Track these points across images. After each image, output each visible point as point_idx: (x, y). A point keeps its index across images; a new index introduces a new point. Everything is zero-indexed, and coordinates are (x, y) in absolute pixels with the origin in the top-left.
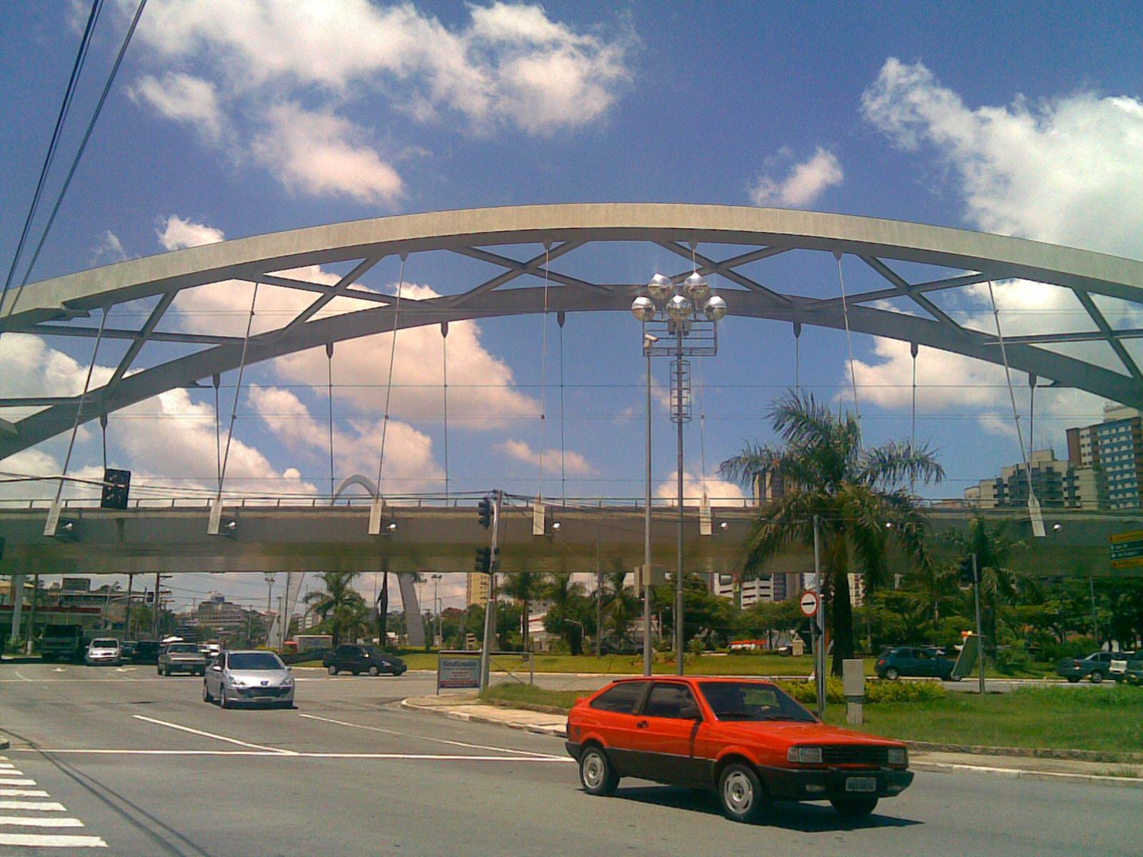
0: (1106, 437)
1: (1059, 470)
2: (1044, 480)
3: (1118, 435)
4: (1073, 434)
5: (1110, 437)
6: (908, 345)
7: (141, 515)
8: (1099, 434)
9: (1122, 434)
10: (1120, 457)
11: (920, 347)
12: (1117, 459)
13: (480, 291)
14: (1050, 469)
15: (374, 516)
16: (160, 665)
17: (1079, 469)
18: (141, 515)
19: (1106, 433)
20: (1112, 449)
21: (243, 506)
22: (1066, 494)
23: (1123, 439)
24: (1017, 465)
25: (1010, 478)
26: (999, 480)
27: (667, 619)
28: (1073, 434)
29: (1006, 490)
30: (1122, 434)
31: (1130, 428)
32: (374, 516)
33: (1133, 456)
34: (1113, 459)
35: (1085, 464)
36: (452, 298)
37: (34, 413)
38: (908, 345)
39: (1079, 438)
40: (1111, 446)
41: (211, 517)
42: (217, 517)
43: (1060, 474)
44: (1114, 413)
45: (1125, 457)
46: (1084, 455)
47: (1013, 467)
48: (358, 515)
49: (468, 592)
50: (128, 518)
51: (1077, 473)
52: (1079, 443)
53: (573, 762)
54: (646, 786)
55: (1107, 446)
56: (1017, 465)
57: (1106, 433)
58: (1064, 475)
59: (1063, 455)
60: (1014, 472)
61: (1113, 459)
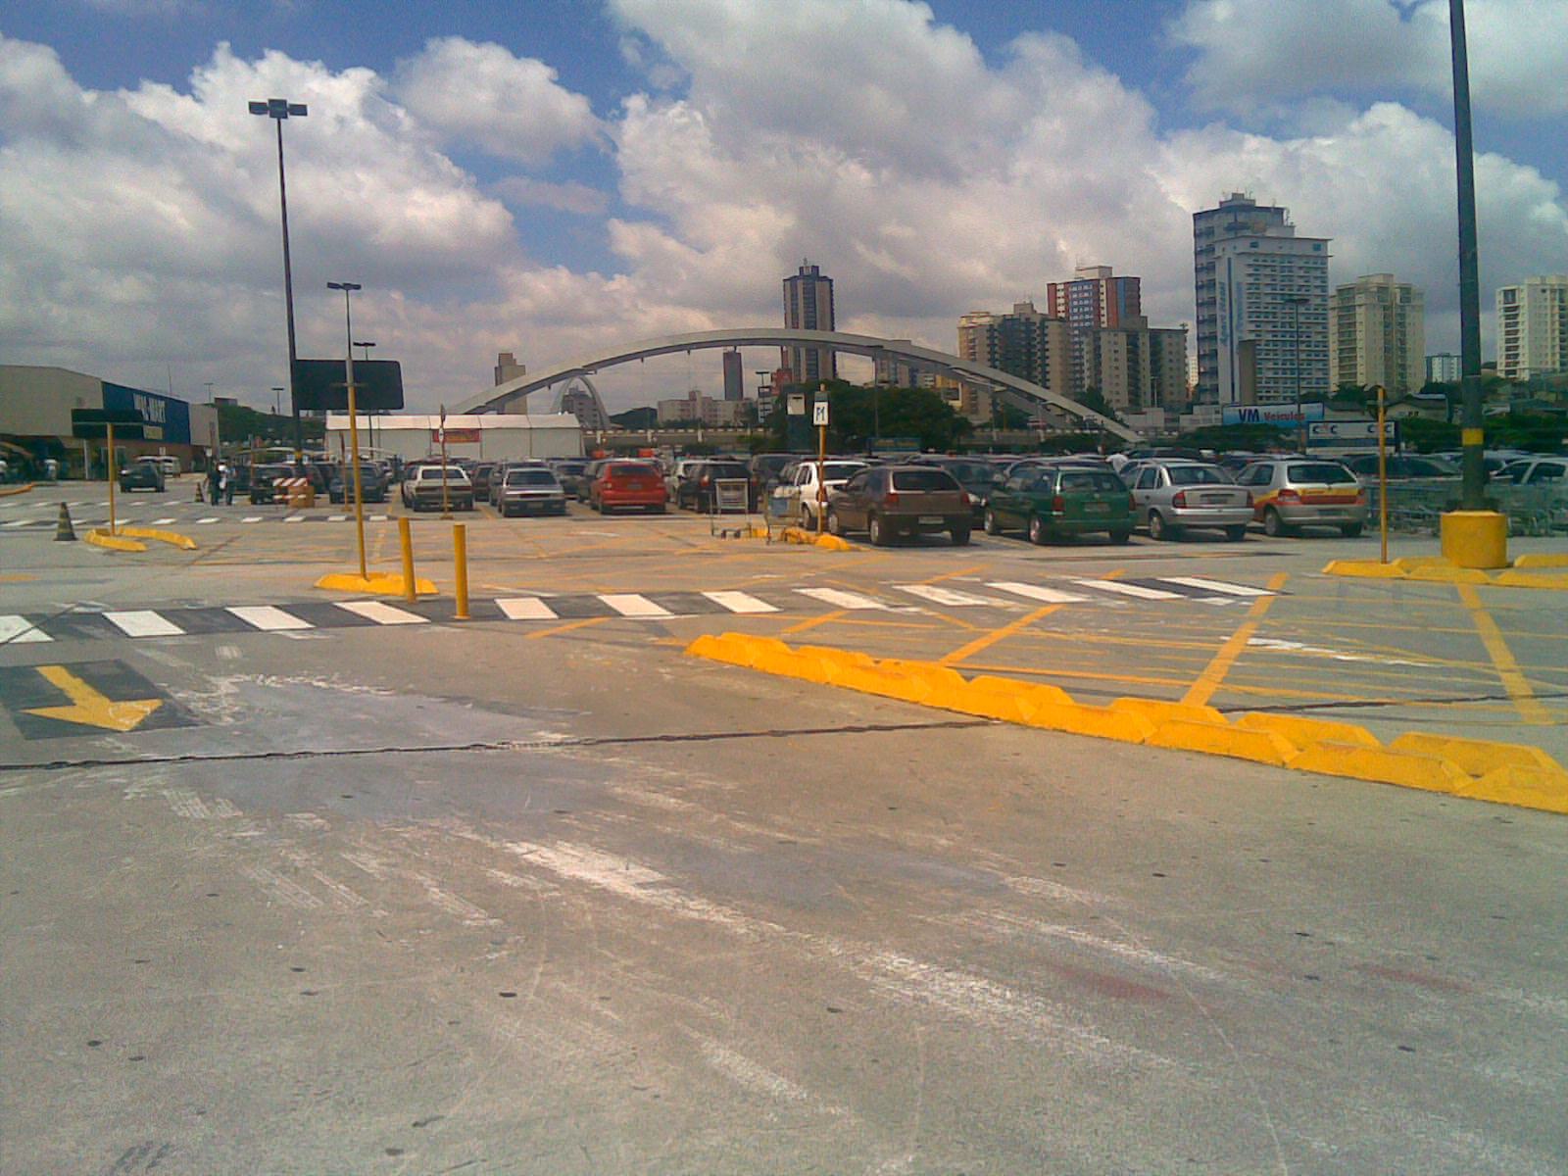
4: (1052, 287)
9: (1086, 291)
16: (1456, 421)
19: (1075, 289)
22: (1039, 346)
25: (999, 325)
28: (1052, 287)
29: (996, 334)
37: (40, 639)
39: (1056, 290)
43: (1035, 323)
49: (1244, 211)
51: (1047, 324)
53: (603, 593)
54: (917, 587)
55: (1074, 300)
57: (1075, 289)
59: (1042, 308)
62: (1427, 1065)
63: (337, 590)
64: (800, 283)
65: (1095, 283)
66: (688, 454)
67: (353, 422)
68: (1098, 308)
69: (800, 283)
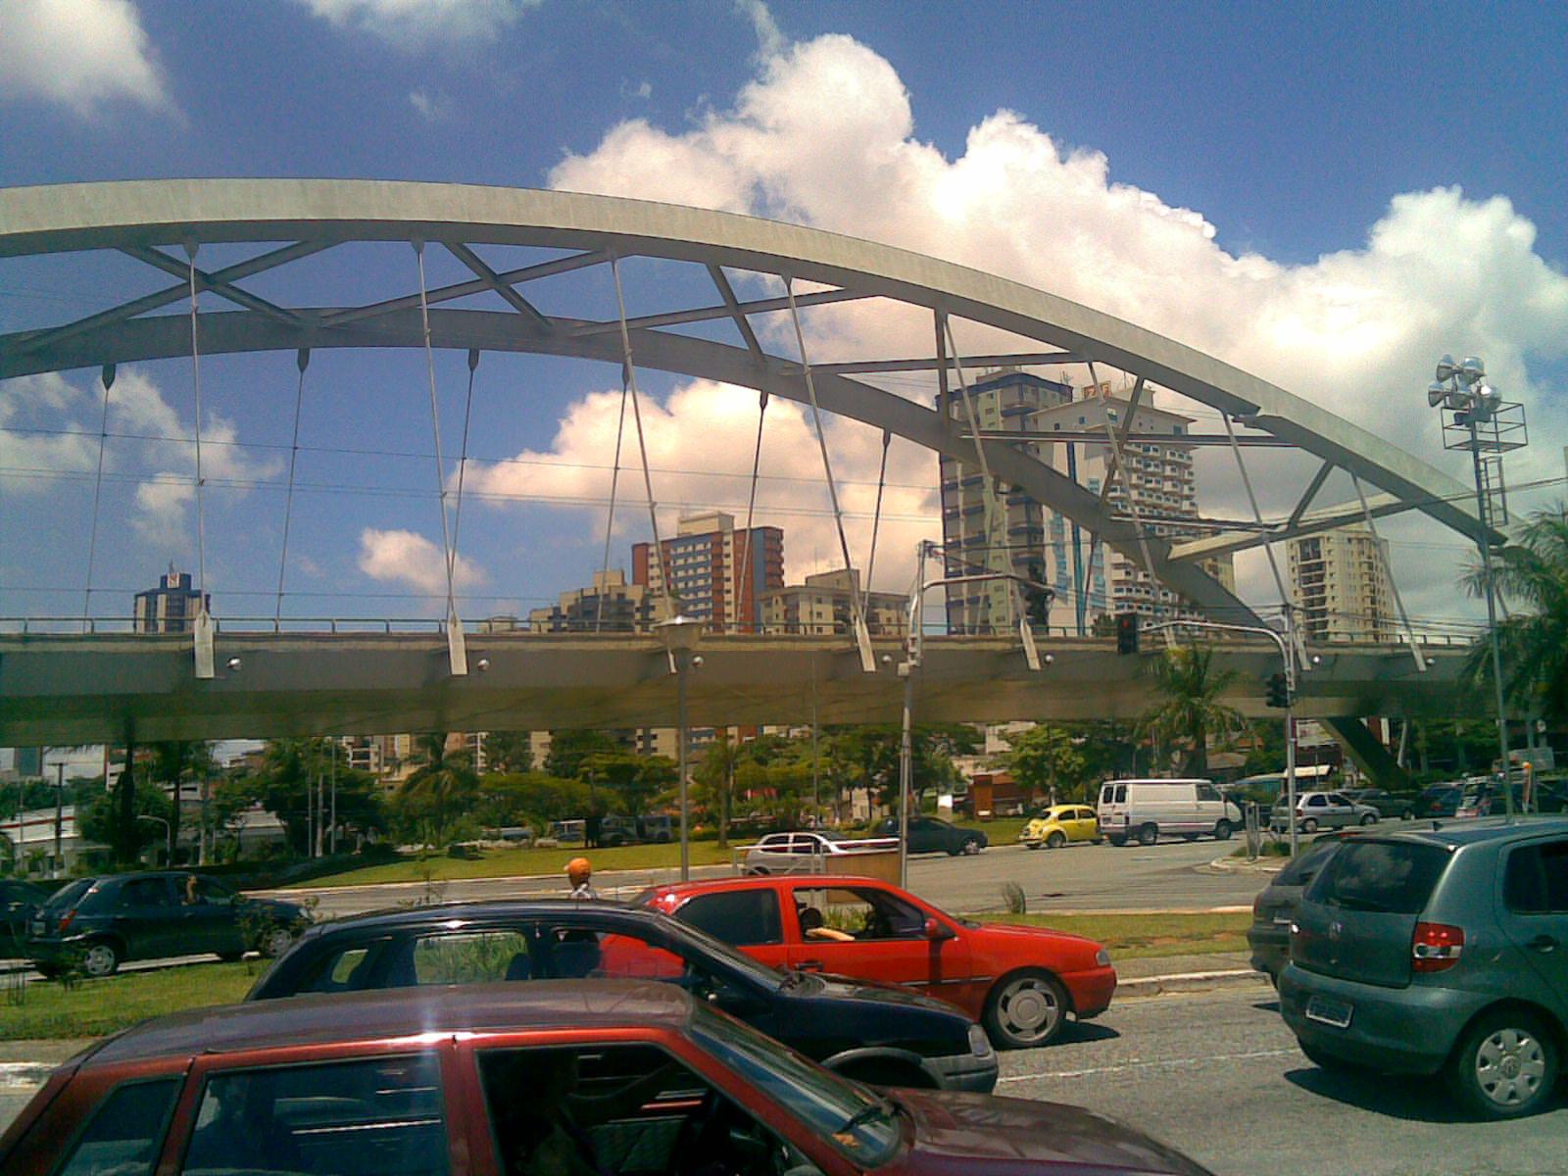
0: (680, 556)
1: (632, 598)
2: (613, 610)
3: (695, 554)
5: (685, 556)
6: (880, 432)
7: (34, 647)
8: (672, 552)
9: (700, 553)
10: (695, 582)
11: (893, 435)
12: (691, 584)
13: (395, 307)
14: (621, 596)
15: (455, 647)
17: (654, 597)
18: (34, 647)
19: (681, 550)
20: (687, 571)
21: (334, 632)
23: (701, 559)
24: (582, 591)
25: (570, 609)
26: (557, 610)
27: (1046, 747)
30: (700, 553)
31: (709, 546)
32: (455, 647)
33: (710, 581)
34: (686, 584)
35: (652, 589)
36: (581, 324)
38: (880, 432)
39: (648, 555)
40: (685, 567)
41: (197, 650)
42: (207, 649)
43: (632, 603)
44: (689, 525)
45: (701, 582)
46: (652, 578)
47: (576, 592)
48: (404, 645)
50: (8, 653)
51: (652, 602)
52: (647, 561)
55: (680, 568)
56: (582, 591)
57: (681, 550)
58: (638, 605)
60: (577, 599)
61: (686, 584)
62: (1157, 721)
63: (209, 1012)
64: (162, 599)
65: (716, 539)
66: (691, 989)
67: (1363, 503)
68: (719, 579)
69: (162, 599)
